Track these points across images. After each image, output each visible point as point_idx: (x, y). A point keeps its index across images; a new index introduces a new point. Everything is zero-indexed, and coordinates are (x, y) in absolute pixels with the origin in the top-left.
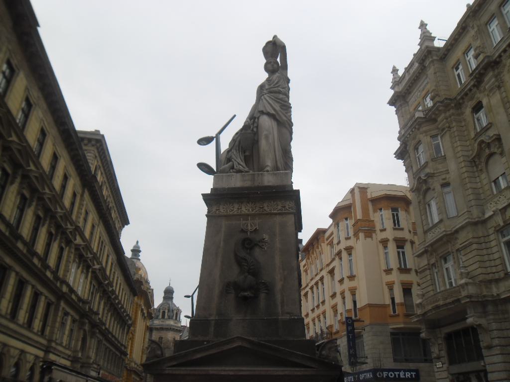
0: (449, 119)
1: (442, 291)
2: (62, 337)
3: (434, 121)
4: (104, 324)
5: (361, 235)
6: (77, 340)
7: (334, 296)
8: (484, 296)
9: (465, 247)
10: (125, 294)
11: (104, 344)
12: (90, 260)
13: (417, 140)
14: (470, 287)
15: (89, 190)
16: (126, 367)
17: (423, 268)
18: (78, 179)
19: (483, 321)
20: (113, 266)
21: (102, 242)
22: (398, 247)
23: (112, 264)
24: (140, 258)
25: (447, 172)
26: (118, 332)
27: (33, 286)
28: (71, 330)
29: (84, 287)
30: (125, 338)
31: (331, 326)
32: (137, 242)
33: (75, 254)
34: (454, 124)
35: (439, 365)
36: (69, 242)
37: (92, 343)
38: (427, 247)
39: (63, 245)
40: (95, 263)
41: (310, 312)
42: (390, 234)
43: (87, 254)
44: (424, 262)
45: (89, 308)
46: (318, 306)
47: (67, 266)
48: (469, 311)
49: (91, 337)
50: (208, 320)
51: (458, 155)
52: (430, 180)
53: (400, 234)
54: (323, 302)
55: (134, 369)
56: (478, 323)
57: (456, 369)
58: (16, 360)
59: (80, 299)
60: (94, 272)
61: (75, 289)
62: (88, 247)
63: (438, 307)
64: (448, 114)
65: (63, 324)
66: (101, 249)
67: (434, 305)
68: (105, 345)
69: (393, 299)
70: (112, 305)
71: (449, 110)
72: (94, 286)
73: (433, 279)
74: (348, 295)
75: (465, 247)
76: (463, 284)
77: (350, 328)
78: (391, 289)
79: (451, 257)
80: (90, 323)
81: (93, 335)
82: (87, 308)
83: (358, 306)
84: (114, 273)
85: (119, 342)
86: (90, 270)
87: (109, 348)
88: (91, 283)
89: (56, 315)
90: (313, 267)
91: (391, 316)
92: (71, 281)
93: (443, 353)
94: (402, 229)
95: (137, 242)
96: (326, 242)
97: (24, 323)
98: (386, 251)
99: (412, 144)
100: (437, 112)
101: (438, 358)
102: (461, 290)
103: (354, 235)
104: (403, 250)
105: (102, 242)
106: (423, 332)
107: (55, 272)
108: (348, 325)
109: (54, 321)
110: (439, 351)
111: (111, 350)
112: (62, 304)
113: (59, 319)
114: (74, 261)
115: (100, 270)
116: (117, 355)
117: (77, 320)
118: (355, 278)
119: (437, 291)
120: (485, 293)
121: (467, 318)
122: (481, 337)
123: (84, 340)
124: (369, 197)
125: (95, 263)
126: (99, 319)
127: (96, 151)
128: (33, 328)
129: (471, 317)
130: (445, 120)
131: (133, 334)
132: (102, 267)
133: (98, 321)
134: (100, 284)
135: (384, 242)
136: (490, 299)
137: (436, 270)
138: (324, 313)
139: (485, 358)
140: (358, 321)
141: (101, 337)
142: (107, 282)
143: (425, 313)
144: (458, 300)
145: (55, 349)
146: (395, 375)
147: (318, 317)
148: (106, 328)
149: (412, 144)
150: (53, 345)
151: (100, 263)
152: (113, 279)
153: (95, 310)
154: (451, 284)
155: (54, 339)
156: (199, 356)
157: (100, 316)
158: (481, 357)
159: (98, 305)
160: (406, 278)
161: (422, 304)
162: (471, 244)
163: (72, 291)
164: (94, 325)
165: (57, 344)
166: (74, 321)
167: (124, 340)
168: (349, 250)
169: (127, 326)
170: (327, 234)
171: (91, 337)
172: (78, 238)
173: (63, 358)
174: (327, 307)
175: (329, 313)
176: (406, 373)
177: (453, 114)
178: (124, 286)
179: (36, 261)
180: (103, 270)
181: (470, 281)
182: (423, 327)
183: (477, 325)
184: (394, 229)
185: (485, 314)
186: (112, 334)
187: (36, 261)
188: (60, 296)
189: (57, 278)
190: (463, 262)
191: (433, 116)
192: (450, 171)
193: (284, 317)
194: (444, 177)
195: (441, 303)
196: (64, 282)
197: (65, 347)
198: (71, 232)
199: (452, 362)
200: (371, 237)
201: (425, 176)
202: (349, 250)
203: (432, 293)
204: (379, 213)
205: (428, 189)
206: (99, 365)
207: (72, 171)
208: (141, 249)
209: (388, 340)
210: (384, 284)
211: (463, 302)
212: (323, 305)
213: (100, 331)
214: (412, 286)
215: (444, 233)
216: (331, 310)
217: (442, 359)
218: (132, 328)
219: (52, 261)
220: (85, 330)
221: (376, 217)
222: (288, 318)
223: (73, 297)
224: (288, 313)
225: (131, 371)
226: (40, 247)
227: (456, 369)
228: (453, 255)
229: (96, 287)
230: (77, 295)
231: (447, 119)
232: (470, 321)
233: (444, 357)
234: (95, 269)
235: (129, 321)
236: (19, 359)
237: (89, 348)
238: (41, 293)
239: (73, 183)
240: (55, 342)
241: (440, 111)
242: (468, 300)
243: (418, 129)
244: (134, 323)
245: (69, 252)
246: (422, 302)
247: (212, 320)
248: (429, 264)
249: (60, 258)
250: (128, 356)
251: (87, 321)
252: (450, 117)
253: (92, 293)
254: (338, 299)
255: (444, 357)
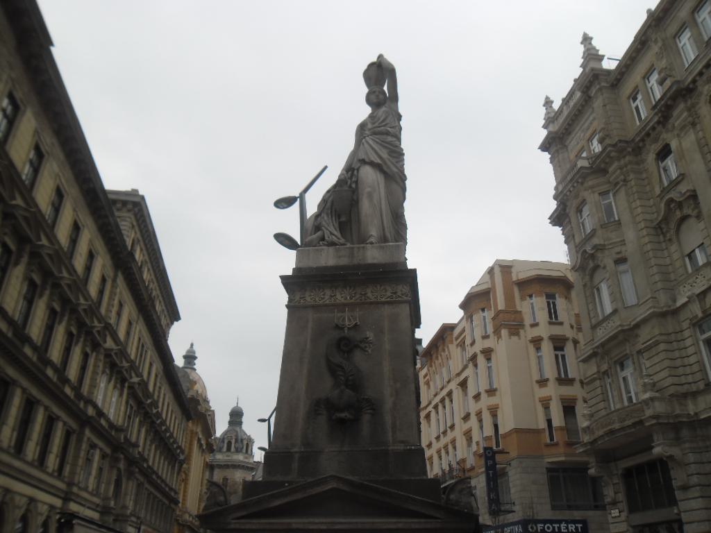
0: (625, 169)
1: (619, 410)
2: (87, 479)
3: (604, 171)
4: (146, 460)
5: (504, 332)
6: (108, 484)
7: (467, 417)
8: (677, 416)
9: (649, 348)
10: (175, 418)
11: (146, 489)
12: (126, 370)
13: (580, 199)
14: (657, 404)
15: (123, 273)
16: (177, 520)
17: (589, 379)
18: (108, 257)
19: (675, 451)
20: (158, 379)
21: (143, 346)
22: (556, 349)
23: (156, 376)
24: (195, 367)
25: (623, 243)
26: (165, 471)
27: (46, 408)
28: (100, 470)
29: (118, 409)
30: (175, 478)
31: (464, 461)
32: (192, 345)
33: (105, 363)
34: (632, 176)
35: (615, 513)
36: (96, 346)
37: (130, 487)
38: (596, 347)
39: (88, 350)
40: (133, 375)
41: (434, 441)
42: (544, 331)
43: (122, 362)
44: (592, 369)
45: (125, 437)
46: (445, 433)
47: (93, 379)
48: (655, 438)
49: (128, 479)
50: (290, 452)
51: (638, 219)
52: (599, 255)
53: (557, 330)
54: (452, 427)
55: (189, 524)
56: (668, 454)
57: (639, 518)
58: (22, 511)
59: (112, 425)
60: (131, 387)
61: (105, 411)
62: (123, 353)
63: (612, 432)
64: (622, 162)
65: (89, 461)
66: (141, 356)
67: (605, 429)
68: (148, 490)
69: (549, 422)
70: (157, 433)
71: (624, 157)
72: (132, 407)
73: (604, 393)
74: (487, 417)
75: (649, 348)
76: (647, 399)
77: (490, 462)
78: (547, 408)
79: (629, 362)
80: (126, 458)
81: (130, 475)
82: (122, 437)
83: (501, 432)
84: (160, 388)
85: (167, 485)
86: (126, 385)
87: (153, 494)
88: (127, 403)
89: (78, 449)
90: (437, 377)
91: (547, 445)
92: (99, 400)
93: (621, 497)
94: (561, 324)
95: (192, 345)
96: (455, 343)
97: (33, 460)
98: (539, 354)
99: (574, 205)
100: (607, 160)
101: (614, 503)
102: (645, 407)
103: (494, 332)
104: (562, 353)
105: (143, 346)
106: (592, 467)
107: (77, 389)
108: (487, 458)
109: (76, 457)
110: (616, 493)
111: (155, 497)
112: (87, 432)
113: (82, 454)
114: (103, 372)
115: (139, 384)
116: (164, 504)
117: (107, 455)
118: (497, 393)
119: (610, 409)
120: (678, 412)
121: (653, 447)
122: (673, 473)
123: (118, 483)
124: (514, 278)
125: (133, 375)
126: (139, 453)
127: (133, 217)
128: (47, 467)
129: (659, 445)
130: (619, 171)
131: (186, 474)
132: (143, 380)
133: (137, 456)
134: (140, 403)
135: (537, 342)
136: (685, 420)
137: (610, 380)
138: (453, 442)
139: (679, 503)
140: (502, 452)
141: (141, 479)
142: (149, 401)
143: (595, 440)
144: (641, 422)
145: (78, 496)
146: (554, 528)
147: (446, 447)
148: (149, 466)
149: (573, 204)
150: (75, 489)
151: (139, 375)
152: (159, 397)
153: (133, 439)
154: (630, 399)
155: (76, 481)
156: (277, 503)
157: (140, 449)
158: (673, 502)
159: (138, 434)
160: (568, 391)
161: (591, 427)
162: (657, 343)
163: (100, 414)
164: (131, 462)
165: (80, 488)
166: (104, 456)
167: (174, 483)
168: (488, 353)
169: (179, 463)
170: (457, 332)
171: (128, 479)
172: (109, 339)
173: (89, 508)
174: (458, 433)
175: (461, 442)
176: (569, 525)
177: (630, 162)
178: (174, 407)
179: (50, 372)
180: (144, 384)
181: (657, 395)
182: (592, 460)
183: (667, 457)
184: (550, 323)
185: (678, 440)
186: (157, 474)
187: (50, 372)
188: (84, 421)
189: (79, 396)
190: (646, 369)
191: (603, 166)
192: (626, 242)
193: (396, 448)
194: (617, 249)
195: (617, 426)
196: (90, 402)
197: (91, 494)
198: (98, 332)
199: (632, 509)
200: (517, 334)
201: (593, 249)
202: (488, 353)
203: (603, 413)
204: (528, 301)
205: (596, 267)
206: (138, 518)
207: (100, 247)
208: (196, 355)
209: (543, 478)
210: (537, 400)
211: (647, 424)
212: (444, 437)
213: (139, 469)
214: (575, 403)
215: (620, 329)
216: (464, 437)
217: (620, 505)
218: (185, 466)
219: (72, 372)
220: (119, 470)
221: (524, 306)
222: (402, 448)
223: (103, 422)
224: (402, 442)
225: (184, 526)
226: (55, 354)
227: (639, 518)
228: (633, 359)
229: (135, 408)
230: (108, 420)
231: (621, 168)
232: (657, 450)
233: (622, 502)
234: (134, 383)
235: (181, 455)
236: (28, 510)
237: (126, 494)
238: (58, 418)
239: (102, 264)
240: (77, 485)
241: (612, 158)
242: (654, 421)
243: (582, 183)
244: (188, 459)
245: (96, 359)
246: (591, 425)
247: (296, 452)
248: (598, 372)
249: (83, 368)
250: (180, 505)
251: (122, 456)
252: (626, 166)
253: (129, 417)
254: (473, 420)
255: (622, 502)
